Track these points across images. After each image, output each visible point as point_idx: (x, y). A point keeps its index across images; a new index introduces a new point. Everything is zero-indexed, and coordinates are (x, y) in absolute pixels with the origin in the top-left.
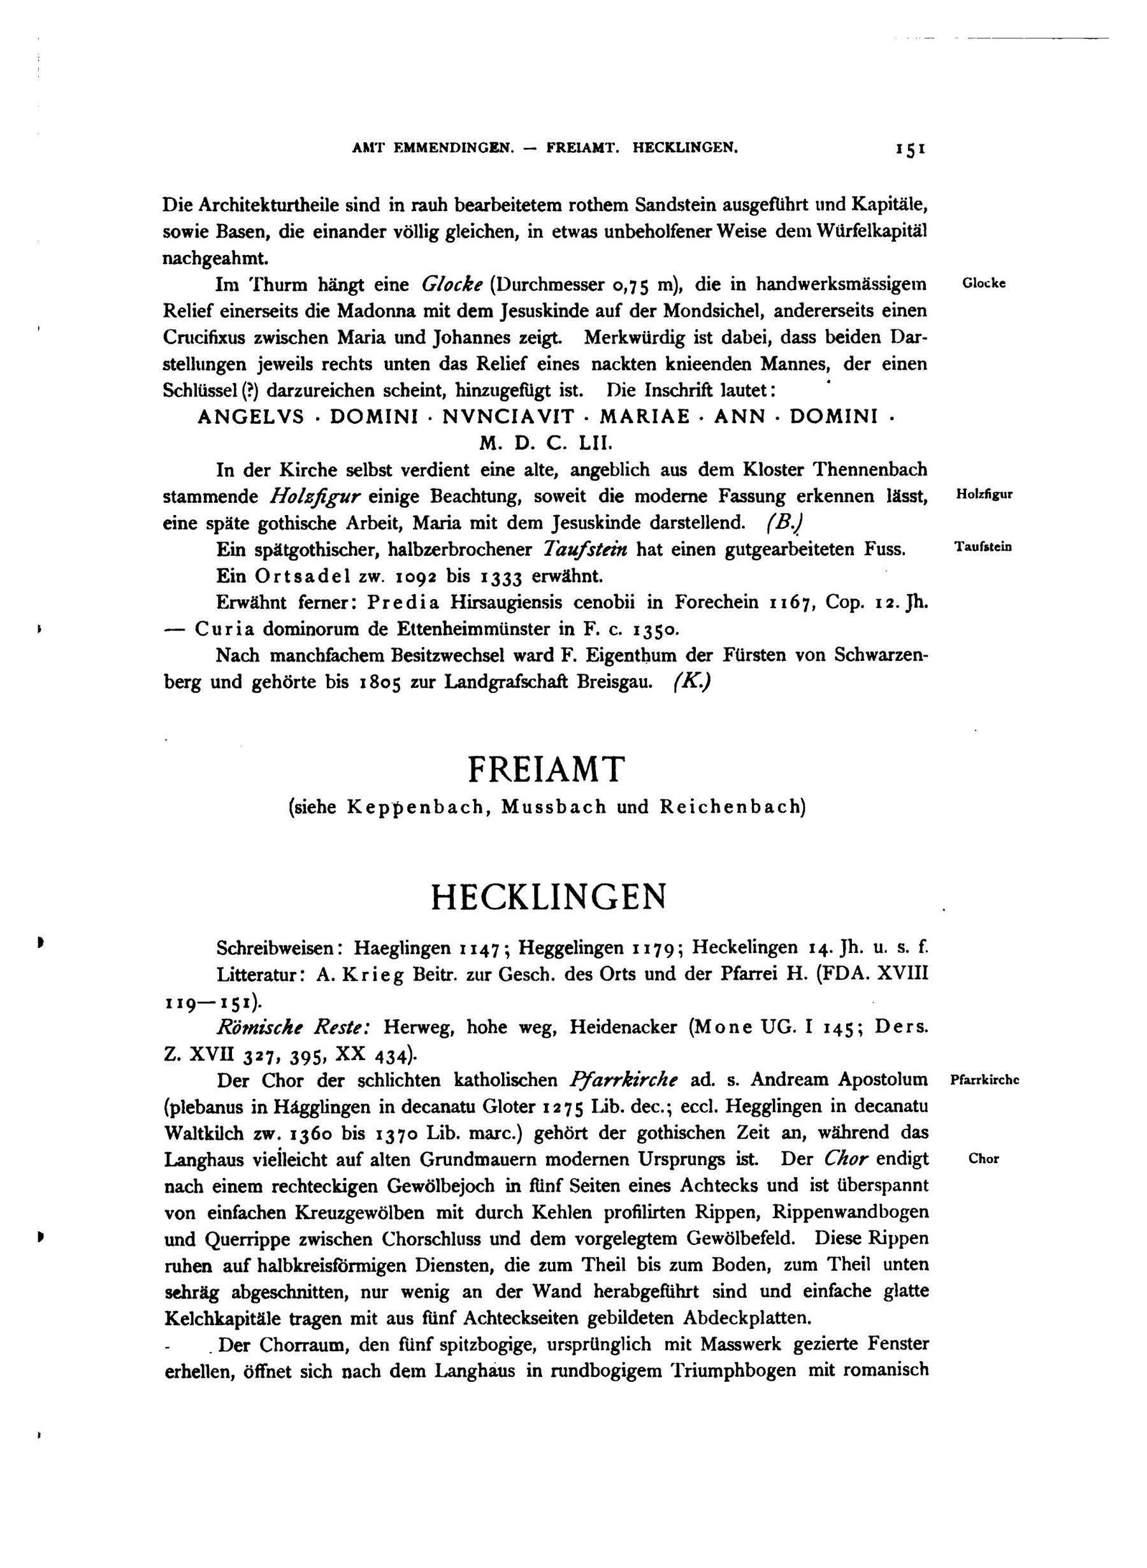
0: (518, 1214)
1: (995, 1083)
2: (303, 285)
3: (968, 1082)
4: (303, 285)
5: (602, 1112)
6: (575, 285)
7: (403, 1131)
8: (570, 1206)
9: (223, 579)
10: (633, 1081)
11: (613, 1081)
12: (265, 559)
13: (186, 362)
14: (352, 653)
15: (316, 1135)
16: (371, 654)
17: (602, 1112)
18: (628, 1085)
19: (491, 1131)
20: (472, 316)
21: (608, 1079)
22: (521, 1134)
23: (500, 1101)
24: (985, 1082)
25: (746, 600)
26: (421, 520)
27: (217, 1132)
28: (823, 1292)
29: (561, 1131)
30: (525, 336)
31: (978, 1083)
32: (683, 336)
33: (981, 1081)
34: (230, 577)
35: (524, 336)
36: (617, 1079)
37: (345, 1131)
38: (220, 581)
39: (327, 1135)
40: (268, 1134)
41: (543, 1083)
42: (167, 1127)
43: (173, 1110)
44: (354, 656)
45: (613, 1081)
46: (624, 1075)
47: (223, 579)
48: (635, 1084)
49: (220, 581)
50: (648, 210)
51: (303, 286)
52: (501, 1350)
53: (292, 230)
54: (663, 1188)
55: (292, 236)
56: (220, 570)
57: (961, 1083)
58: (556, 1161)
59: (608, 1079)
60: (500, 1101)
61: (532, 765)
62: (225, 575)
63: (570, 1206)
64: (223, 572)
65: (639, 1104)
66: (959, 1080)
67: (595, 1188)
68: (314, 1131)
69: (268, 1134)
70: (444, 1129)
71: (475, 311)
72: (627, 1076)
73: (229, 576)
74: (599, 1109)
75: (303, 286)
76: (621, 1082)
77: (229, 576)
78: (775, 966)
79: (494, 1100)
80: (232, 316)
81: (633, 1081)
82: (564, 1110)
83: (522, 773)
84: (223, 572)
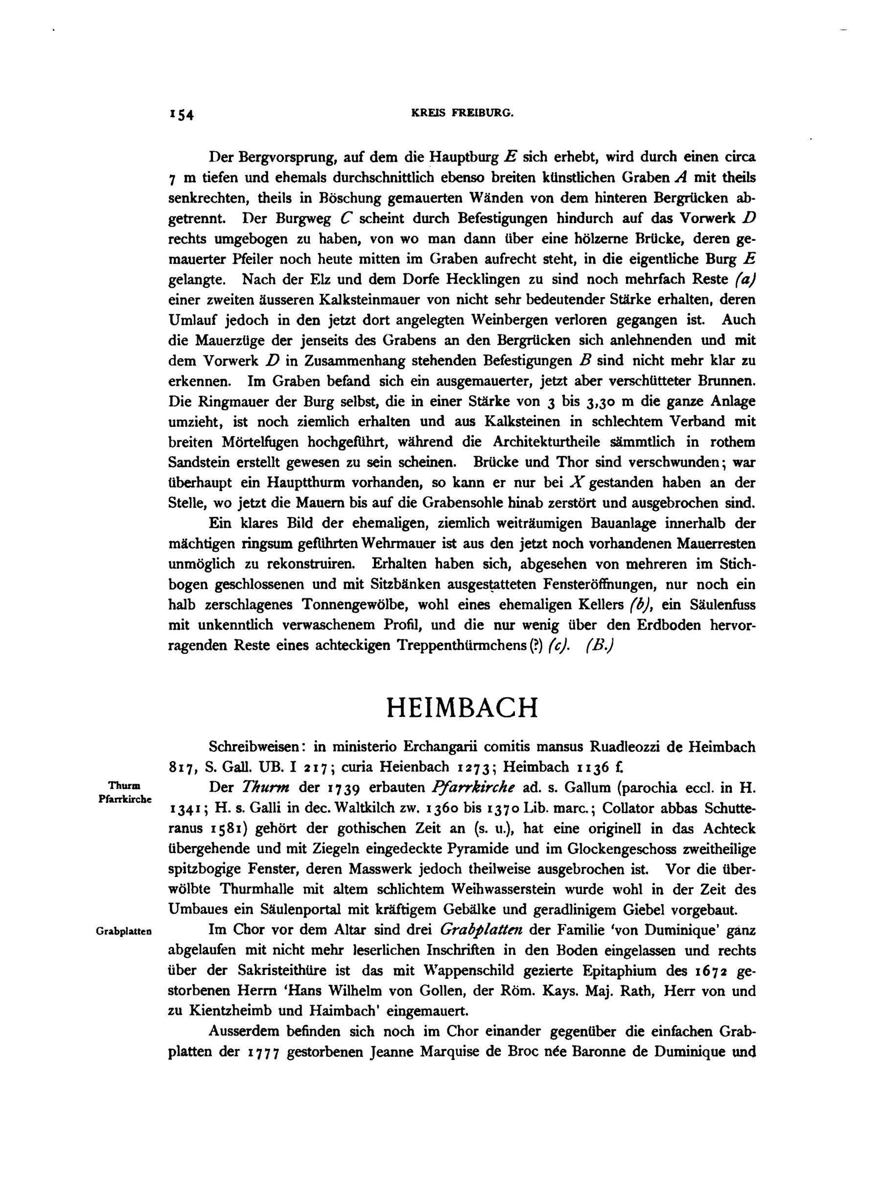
0: (724, 585)
1: (133, 802)
2: (364, 890)
3: (112, 801)
4: (364, 890)
5: (532, 812)
6: (605, 483)
7: (508, 806)
8: (494, 498)
9: (214, 525)
10: (480, 788)
11: (465, 788)
12: (413, 925)
13: (261, 441)
14: (399, 948)
15: (446, 809)
16: (317, 420)
17: (532, 812)
18: (477, 791)
19: (635, 786)
20: (263, 1035)
21: (461, 787)
22: (246, 829)
23: (581, 844)
24: (125, 801)
25: (671, 603)
26: (355, 866)
27: (374, 806)
28: (581, 911)
29: (580, 237)
30: (553, 502)
31: (120, 802)
32: (557, 624)
33: (122, 800)
34: (220, 524)
35: (552, 502)
36: (468, 787)
37: (466, 806)
38: (212, 527)
39: (454, 809)
40: (412, 809)
41: (202, 424)
42: (337, 803)
43: (639, 824)
44: (401, 950)
45: (465, 788)
46: (474, 784)
47: (214, 525)
48: (482, 791)
49: (212, 527)
50: (270, 913)
51: (364, 890)
52: (186, 954)
53: (415, 156)
54: (682, 972)
55: (396, 405)
56: (212, 518)
57: (107, 802)
58: (254, 951)
59: (461, 787)
60: (581, 844)
61: (424, 704)
62: (215, 522)
63: (494, 498)
64: (214, 520)
65: (311, 806)
66: (105, 800)
67: (234, 302)
68: (444, 806)
69: (412, 809)
70: (537, 805)
71: (266, 1031)
72: (476, 785)
73: (218, 523)
74: (529, 810)
75: (364, 890)
76: (471, 789)
77: (218, 523)
78: (658, 741)
79: (576, 844)
80: (375, 852)
81: (480, 788)
82: (474, 769)
83: (416, 710)
84: (214, 520)
